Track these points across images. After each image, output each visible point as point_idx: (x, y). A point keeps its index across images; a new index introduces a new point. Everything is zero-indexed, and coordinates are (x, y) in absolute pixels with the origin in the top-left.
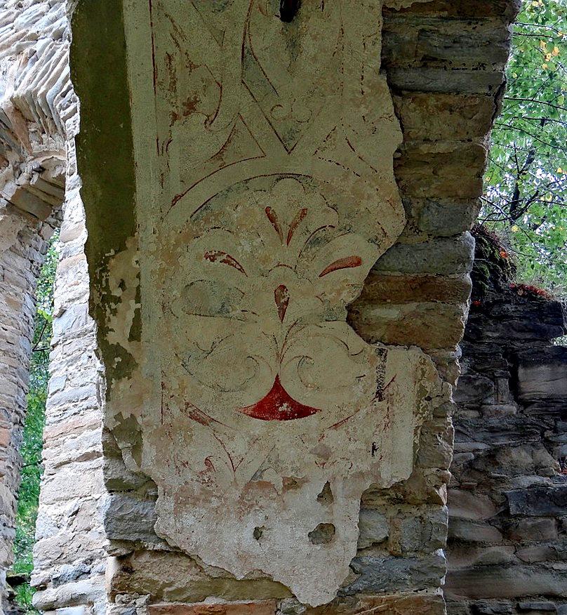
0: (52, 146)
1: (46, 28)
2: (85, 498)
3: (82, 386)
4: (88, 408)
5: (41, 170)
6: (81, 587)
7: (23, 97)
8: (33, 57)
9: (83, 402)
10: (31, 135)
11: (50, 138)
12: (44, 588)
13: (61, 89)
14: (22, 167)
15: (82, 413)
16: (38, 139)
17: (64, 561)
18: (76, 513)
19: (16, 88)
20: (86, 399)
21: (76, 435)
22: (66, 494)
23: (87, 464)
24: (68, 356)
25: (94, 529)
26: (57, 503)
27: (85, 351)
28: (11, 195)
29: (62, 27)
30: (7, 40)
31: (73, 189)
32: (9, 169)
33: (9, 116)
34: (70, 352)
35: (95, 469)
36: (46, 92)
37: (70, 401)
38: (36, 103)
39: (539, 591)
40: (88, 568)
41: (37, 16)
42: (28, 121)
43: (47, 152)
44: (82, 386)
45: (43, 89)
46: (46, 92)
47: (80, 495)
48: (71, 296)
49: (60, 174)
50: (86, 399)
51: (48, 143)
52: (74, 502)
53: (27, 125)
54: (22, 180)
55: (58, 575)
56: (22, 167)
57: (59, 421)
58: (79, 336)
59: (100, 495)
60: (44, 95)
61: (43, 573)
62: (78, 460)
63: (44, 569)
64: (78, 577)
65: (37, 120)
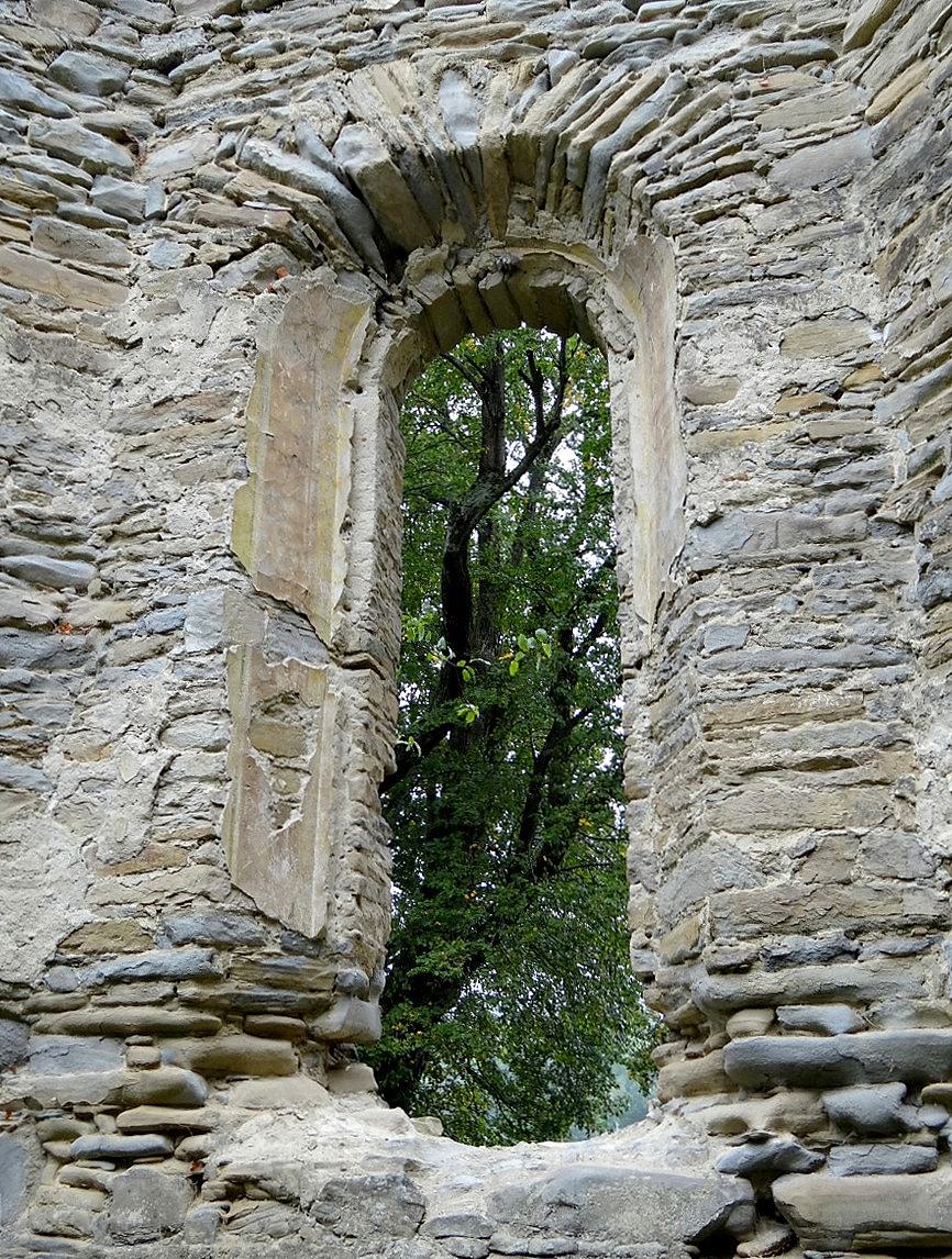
0: (554, 233)
1: (567, 33)
2: (829, 832)
3: (786, 647)
4: (809, 685)
5: (511, 270)
6: (843, 973)
7: (537, 139)
8: (541, 75)
9: (794, 675)
10: (514, 206)
11: (555, 221)
12: (746, 971)
13: (632, 145)
14: (464, 255)
15: (795, 691)
16: (525, 215)
17: (793, 929)
18: (809, 853)
19: (517, 119)
20: (802, 669)
21: (786, 727)
22: (782, 821)
23: (817, 777)
24: (746, 594)
25: (859, 883)
26: (760, 833)
27: (784, 592)
28: (434, 297)
29: (613, 39)
30: (474, 30)
31: (697, 318)
32: (442, 252)
33: (488, 164)
34: (747, 588)
35: (844, 786)
36: (591, 143)
37: (763, 669)
38: (559, 155)
39: (804, 989)
40: (854, 945)
41: (544, 7)
42: (515, 180)
43: (542, 243)
44: (786, 647)
45: (583, 137)
46: (591, 143)
47: (818, 825)
48: (734, 495)
49: (556, 285)
50: (802, 669)
51: (548, 228)
52: (806, 833)
53: (511, 186)
54: (462, 276)
55: (784, 951)
56: (464, 255)
57: (740, 699)
58: (763, 565)
59: (866, 830)
60: (586, 148)
61: (743, 945)
62: (798, 767)
63: (743, 939)
64: (832, 958)
65: (540, 182)
